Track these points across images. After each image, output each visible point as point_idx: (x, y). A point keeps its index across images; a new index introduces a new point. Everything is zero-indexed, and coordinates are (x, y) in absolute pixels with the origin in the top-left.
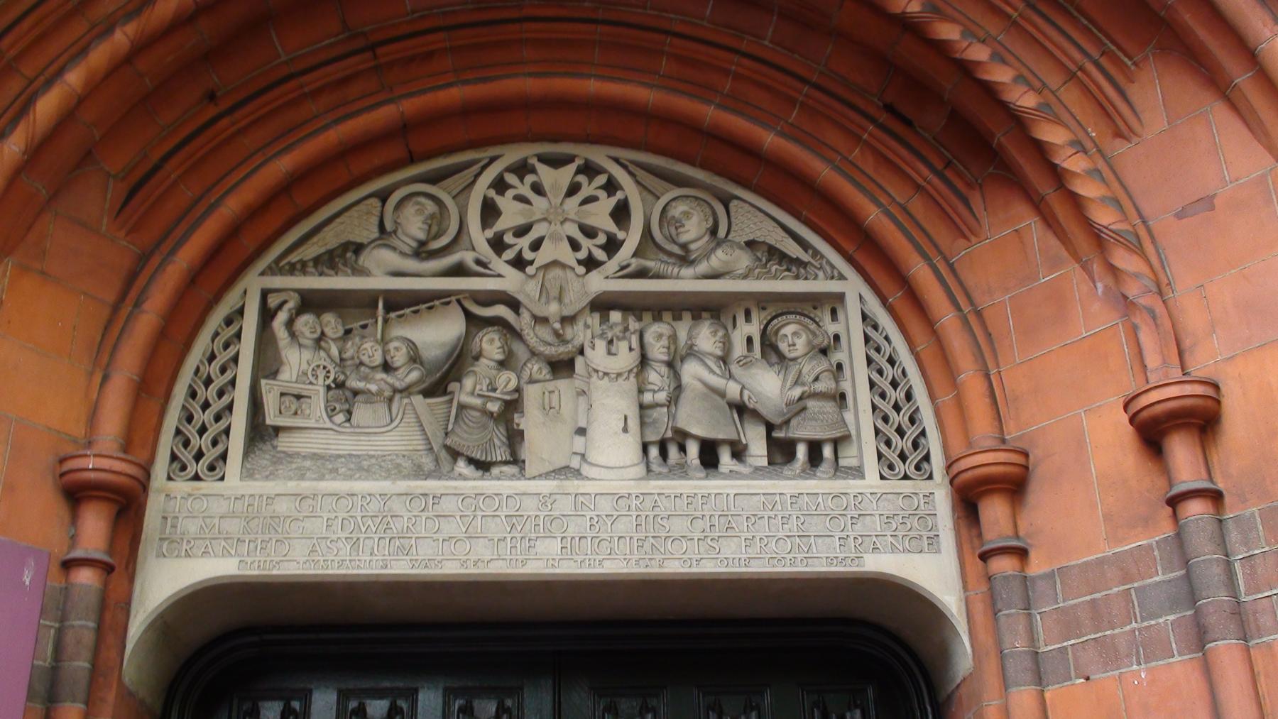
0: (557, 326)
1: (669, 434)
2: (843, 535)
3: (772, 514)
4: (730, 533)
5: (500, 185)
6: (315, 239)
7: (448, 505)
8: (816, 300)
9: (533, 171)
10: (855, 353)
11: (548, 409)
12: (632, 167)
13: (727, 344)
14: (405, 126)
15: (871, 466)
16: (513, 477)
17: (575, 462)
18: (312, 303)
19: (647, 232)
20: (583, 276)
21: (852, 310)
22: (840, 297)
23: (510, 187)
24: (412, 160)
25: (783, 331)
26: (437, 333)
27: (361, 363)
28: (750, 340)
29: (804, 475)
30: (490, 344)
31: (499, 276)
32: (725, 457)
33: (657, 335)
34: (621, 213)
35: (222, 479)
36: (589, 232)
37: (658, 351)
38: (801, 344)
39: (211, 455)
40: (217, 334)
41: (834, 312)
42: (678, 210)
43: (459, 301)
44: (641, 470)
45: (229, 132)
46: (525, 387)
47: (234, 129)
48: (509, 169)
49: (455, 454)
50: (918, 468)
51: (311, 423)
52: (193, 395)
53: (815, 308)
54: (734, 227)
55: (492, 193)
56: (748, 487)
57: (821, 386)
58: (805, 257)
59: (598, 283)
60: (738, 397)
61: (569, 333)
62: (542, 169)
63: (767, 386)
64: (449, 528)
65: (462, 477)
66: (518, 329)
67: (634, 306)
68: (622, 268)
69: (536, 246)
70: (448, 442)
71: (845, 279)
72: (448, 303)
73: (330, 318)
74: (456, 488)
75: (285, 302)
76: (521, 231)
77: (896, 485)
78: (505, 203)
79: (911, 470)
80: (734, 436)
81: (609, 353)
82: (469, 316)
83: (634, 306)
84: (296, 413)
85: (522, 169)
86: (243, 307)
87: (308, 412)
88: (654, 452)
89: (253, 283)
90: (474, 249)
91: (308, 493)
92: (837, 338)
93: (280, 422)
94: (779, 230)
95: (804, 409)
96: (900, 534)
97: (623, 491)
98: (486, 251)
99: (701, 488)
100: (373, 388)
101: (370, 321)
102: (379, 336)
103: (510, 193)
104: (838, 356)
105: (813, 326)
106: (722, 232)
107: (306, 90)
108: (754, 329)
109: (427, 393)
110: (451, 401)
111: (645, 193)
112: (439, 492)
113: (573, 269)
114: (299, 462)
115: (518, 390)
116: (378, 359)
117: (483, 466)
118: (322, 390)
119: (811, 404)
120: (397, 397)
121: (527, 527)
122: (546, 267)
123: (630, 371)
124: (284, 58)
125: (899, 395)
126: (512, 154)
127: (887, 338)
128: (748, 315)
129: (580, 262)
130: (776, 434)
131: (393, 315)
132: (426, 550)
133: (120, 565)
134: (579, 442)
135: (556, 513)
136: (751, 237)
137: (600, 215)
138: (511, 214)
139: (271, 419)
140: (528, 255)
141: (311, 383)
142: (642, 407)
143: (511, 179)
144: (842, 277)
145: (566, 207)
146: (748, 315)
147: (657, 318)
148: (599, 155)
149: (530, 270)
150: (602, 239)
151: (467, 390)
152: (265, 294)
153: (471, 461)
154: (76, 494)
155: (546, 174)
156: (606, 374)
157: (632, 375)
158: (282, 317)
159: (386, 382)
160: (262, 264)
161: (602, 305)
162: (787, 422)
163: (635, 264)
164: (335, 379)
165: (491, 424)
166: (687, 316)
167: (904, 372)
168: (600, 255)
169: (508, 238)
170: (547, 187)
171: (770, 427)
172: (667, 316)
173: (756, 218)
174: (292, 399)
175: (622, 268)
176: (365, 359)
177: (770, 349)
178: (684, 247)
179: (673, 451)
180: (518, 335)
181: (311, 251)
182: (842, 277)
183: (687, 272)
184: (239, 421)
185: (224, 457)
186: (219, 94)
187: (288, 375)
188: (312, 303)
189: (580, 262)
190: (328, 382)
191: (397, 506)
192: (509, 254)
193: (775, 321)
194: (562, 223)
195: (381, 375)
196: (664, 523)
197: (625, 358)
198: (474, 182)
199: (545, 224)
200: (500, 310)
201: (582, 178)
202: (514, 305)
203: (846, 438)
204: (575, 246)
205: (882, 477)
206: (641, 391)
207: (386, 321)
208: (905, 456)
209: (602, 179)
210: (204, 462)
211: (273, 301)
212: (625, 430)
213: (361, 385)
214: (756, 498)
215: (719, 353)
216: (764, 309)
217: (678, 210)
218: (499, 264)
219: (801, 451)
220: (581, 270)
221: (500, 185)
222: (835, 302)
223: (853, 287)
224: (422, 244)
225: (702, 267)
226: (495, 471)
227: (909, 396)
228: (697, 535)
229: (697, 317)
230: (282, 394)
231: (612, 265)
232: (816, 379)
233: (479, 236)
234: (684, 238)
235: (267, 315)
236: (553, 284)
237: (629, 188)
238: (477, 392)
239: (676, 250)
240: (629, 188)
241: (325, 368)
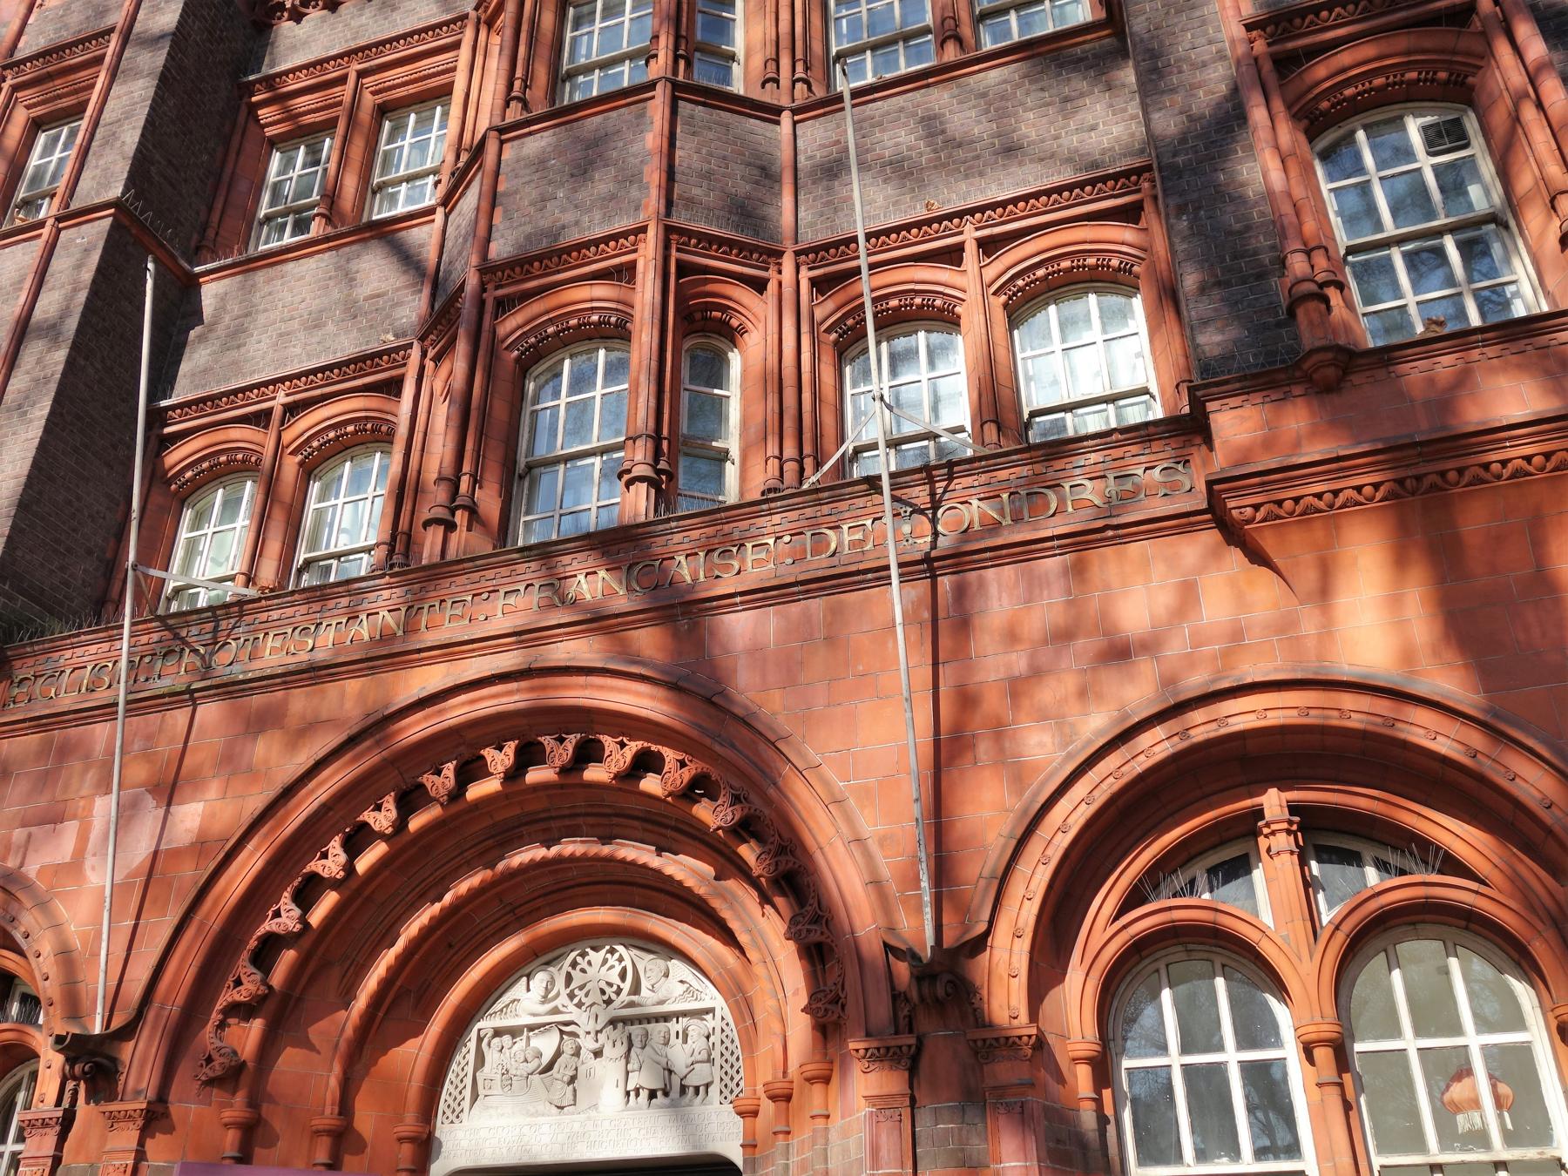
18: (498, 1033)
32: (659, 1094)
33: (636, 1030)
37: (637, 1042)
69: (587, 995)
78: (576, 974)
82: (562, 1032)
98: (566, 1001)
139: (481, 1091)
158: (486, 1041)
184: (467, 1093)
187: (487, 1068)
188: (498, 1033)
209: (579, 959)
218: (571, 1007)
233: (564, 992)
235: (480, 1040)
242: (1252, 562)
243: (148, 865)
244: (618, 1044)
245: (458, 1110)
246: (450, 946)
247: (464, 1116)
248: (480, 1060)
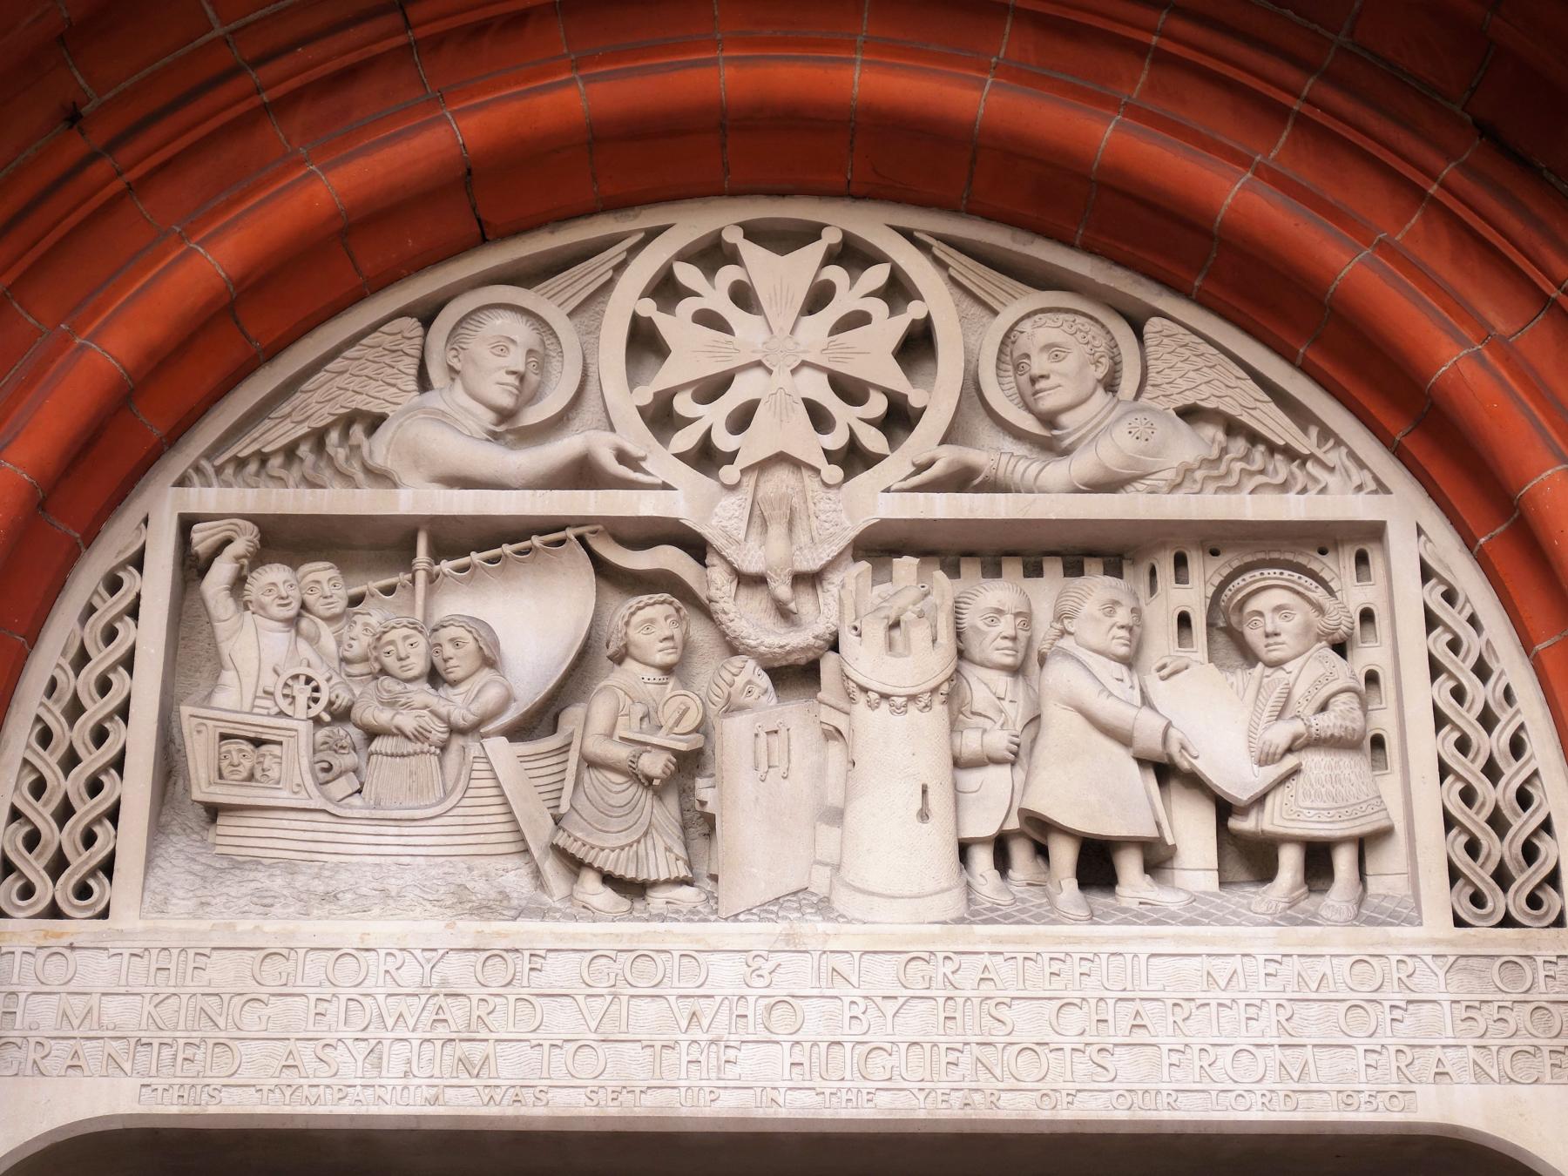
0: (783, 590)
1: (1014, 824)
2: (1373, 1043)
3: (1225, 997)
4: (1140, 1036)
5: (666, 289)
6: (286, 408)
7: (560, 972)
8: (1324, 537)
9: (733, 257)
10: (1403, 647)
11: (764, 767)
12: (939, 249)
13: (1136, 636)
14: (469, 171)
15: (1437, 897)
16: (693, 915)
17: (820, 881)
18: (284, 540)
19: (972, 389)
20: (838, 486)
21: (1402, 552)
22: (1376, 532)
23: (683, 293)
24: (484, 237)
25: (1254, 605)
26: (532, 620)
27: (384, 671)
28: (1184, 621)
29: (1290, 917)
30: (650, 624)
31: (665, 486)
32: (1129, 866)
33: (995, 597)
34: (917, 347)
35: (104, 914)
36: (850, 390)
37: (993, 643)
38: (1289, 628)
39: (81, 862)
40: (91, 610)
41: (1362, 559)
42: (1038, 334)
43: (581, 539)
44: (953, 903)
45: (108, 192)
46: (716, 722)
47: (118, 185)
48: (685, 256)
49: (574, 865)
50: (1534, 902)
51: (283, 797)
52: (45, 737)
53: (1323, 552)
54: (1152, 374)
55: (648, 308)
56: (1178, 939)
57: (1327, 723)
58: (1305, 443)
59: (879, 498)
60: (1159, 748)
61: (804, 604)
62: (751, 252)
63: (1218, 721)
64: (561, 1020)
65: (590, 913)
66: (703, 596)
67: (949, 550)
68: (921, 468)
69: (742, 420)
70: (561, 840)
71: (1387, 491)
72: (561, 542)
73: (321, 573)
74: (574, 937)
75: (228, 541)
76: (712, 389)
77: (1485, 937)
78: (675, 326)
79: (1519, 909)
80: (1148, 831)
81: (890, 645)
82: (602, 568)
83: (949, 550)
84: (251, 777)
85: (712, 254)
86: (142, 551)
87: (274, 774)
88: (983, 859)
89: (161, 506)
90: (613, 429)
91: (274, 945)
92: (1367, 616)
93: (221, 795)
94: (1250, 384)
95: (1295, 772)
96: (1493, 1042)
97: (918, 948)
98: (637, 437)
99: (1078, 940)
100: (407, 721)
101: (404, 577)
102: (419, 616)
103: (687, 307)
104: (1369, 655)
105: (1319, 594)
106: (1128, 384)
107: (265, 97)
108: (1193, 596)
109: (519, 732)
110: (565, 749)
111: (966, 302)
112: (541, 946)
113: (817, 471)
114: (262, 879)
115: (702, 728)
116: (418, 665)
117: (632, 889)
118: (304, 728)
119: (1315, 763)
120: (457, 742)
121: (723, 1018)
122: (763, 466)
123: (934, 691)
124: (219, 31)
125: (1498, 741)
126: (691, 224)
127: (1473, 620)
128: (1181, 562)
129: (830, 456)
130: (1235, 823)
131: (446, 566)
132: (510, 1066)
134: (829, 836)
135: (779, 992)
136: (1190, 399)
137: (872, 355)
138: (690, 352)
139: (204, 788)
140: (724, 441)
141: (281, 714)
142: (958, 763)
143: (688, 274)
144: (1382, 488)
145: (801, 334)
146: (1181, 562)
147: (993, 569)
148: (871, 224)
149: (729, 473)
150: (877, 405)
151: (596, 721)
152: (187, 524)
153: (608, 879)
155: (758, 262)
156: (885, 696)
157: (938, 698)
158: (222, 571)
159: (434, 713)
160: (179, 462)
161: (879, 547)
162: (1260, 800)
163: (946, 458)
164: (331, 703)
165: (647, 799)
166: (1053, 568)
167: (1508, 694)
168: (873, 440)
169: (684, 405)
170: (763, 293)
171: (1224, 809)
172: (1012, 568)
173: (1198, 357)
174: (248, 747)
175: (921, 468)
176: (391, 662)
177: (1232, 639)
178: (1049, 420)
179: (1021, 854)
180: (704, 609)
181: (276, 434)
182: (1382, 488)
183: (1058, 471)
184: (135, 790)
185: (107, 867)
186: (85, 110)
187: (234, 697)
188: (284, 540)
189: (830, 456)
190: (317, 709)
191: (457, 970)
192: (686, 440)
193: (1239, 582)
194: (794, 372)
195: (422, 693)
196: (1003, 1013)
197: (924, 662)
198: (608, 286)
199: (758, 374)
200: (668, 558)
201: (836, 274)
202: (697, 547)
203: (1384, 834)
204: (820, 418)
205: (1459, 922)
206: (954, 727)
207: (432, 579)
209: (877, 276)
210: (69, 879)
211: (202, 538)
212: (924, 815)
213: (383, 717)
214: (1195, 962)
215: (1123, 651)
216: (1215, 553)
217: (1038, 334)
218: (662, 461)
219: (1290, 861)
220: (834, 473)
221: (666, 289)
222: (1362, 541)
224: (505, 416)
225: (1081, 465)
226: (657, 899)
227: (1517, 747)
228: (1069, 1041)
229: (1074, 568)
230: (224, 737)
231: (896, 465)
232: (1323, 708)
233: (624, 398)
234: (1048, 402)
235: (192, 567)
236: (777, 520)
237: (935, 298)
238: (621, 732)
239: (1029, 424)
240: (935, 298)
241: (309, 680)
242: (783, 252)
243: (958, 293)
244: (919, 634)
245: (81, 862)
246: (73, 118)
247: (123, 891)
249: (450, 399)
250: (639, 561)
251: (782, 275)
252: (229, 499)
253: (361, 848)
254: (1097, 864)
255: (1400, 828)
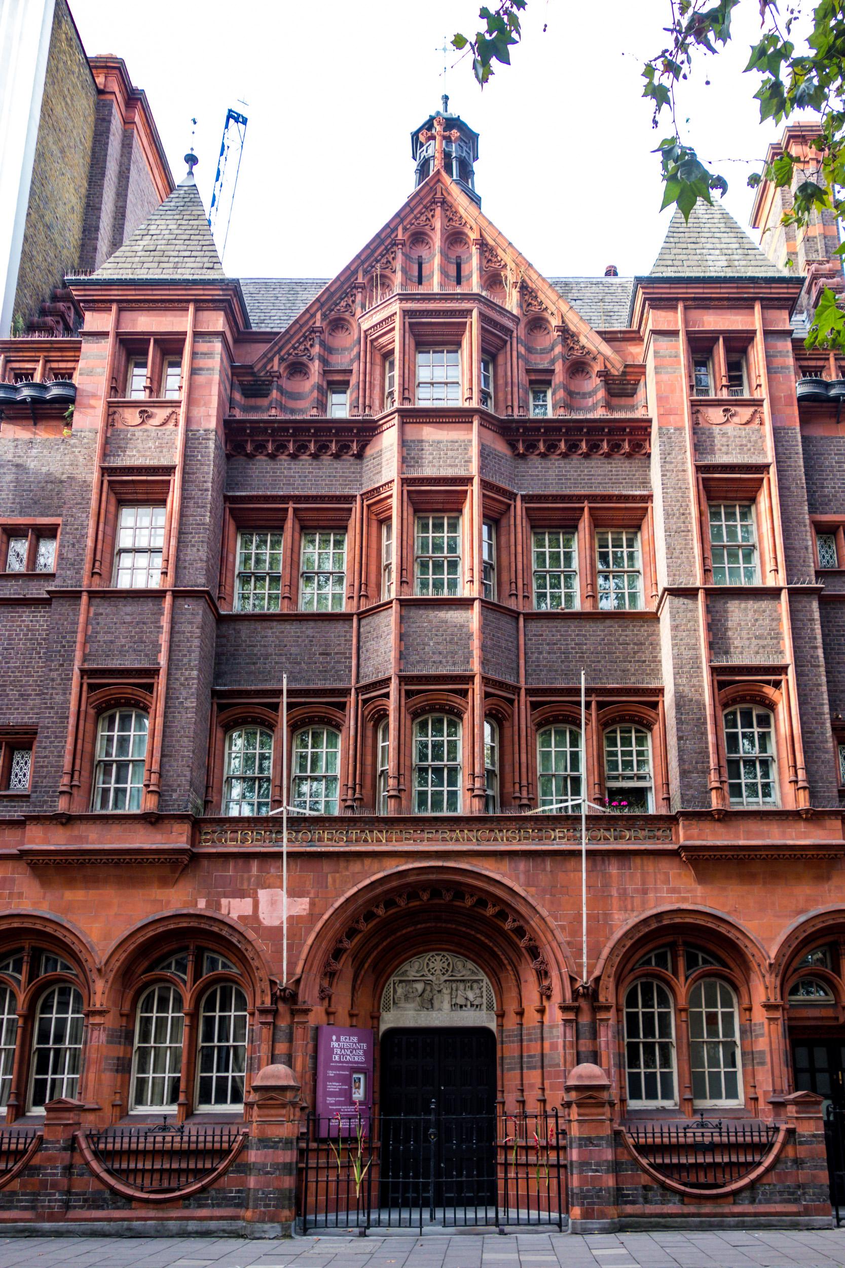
10: (484, 989)
18: (401, 982)
21: (484, 984)
26: (420, 987)
33: (454, 985)
59: (446, 978)
63: (471, 995)
89: (392, 979)
126: (431, 954)
133: (378, 1028)
137: (445, 965)
151: (425, 995)
154: (372, 1018)
161: (446, 981)
173: (470, 965)
188: (401, 982)
208: (490, 1007)
223: (485, 979)
236: (437, 979)
248: (395, 991)
249: (412, 969)
250: (427, 983)
251: (438, 958)
252: (397, 979)
253: (408, 1006)
254: (461, 1006)
255: (757, 545)
